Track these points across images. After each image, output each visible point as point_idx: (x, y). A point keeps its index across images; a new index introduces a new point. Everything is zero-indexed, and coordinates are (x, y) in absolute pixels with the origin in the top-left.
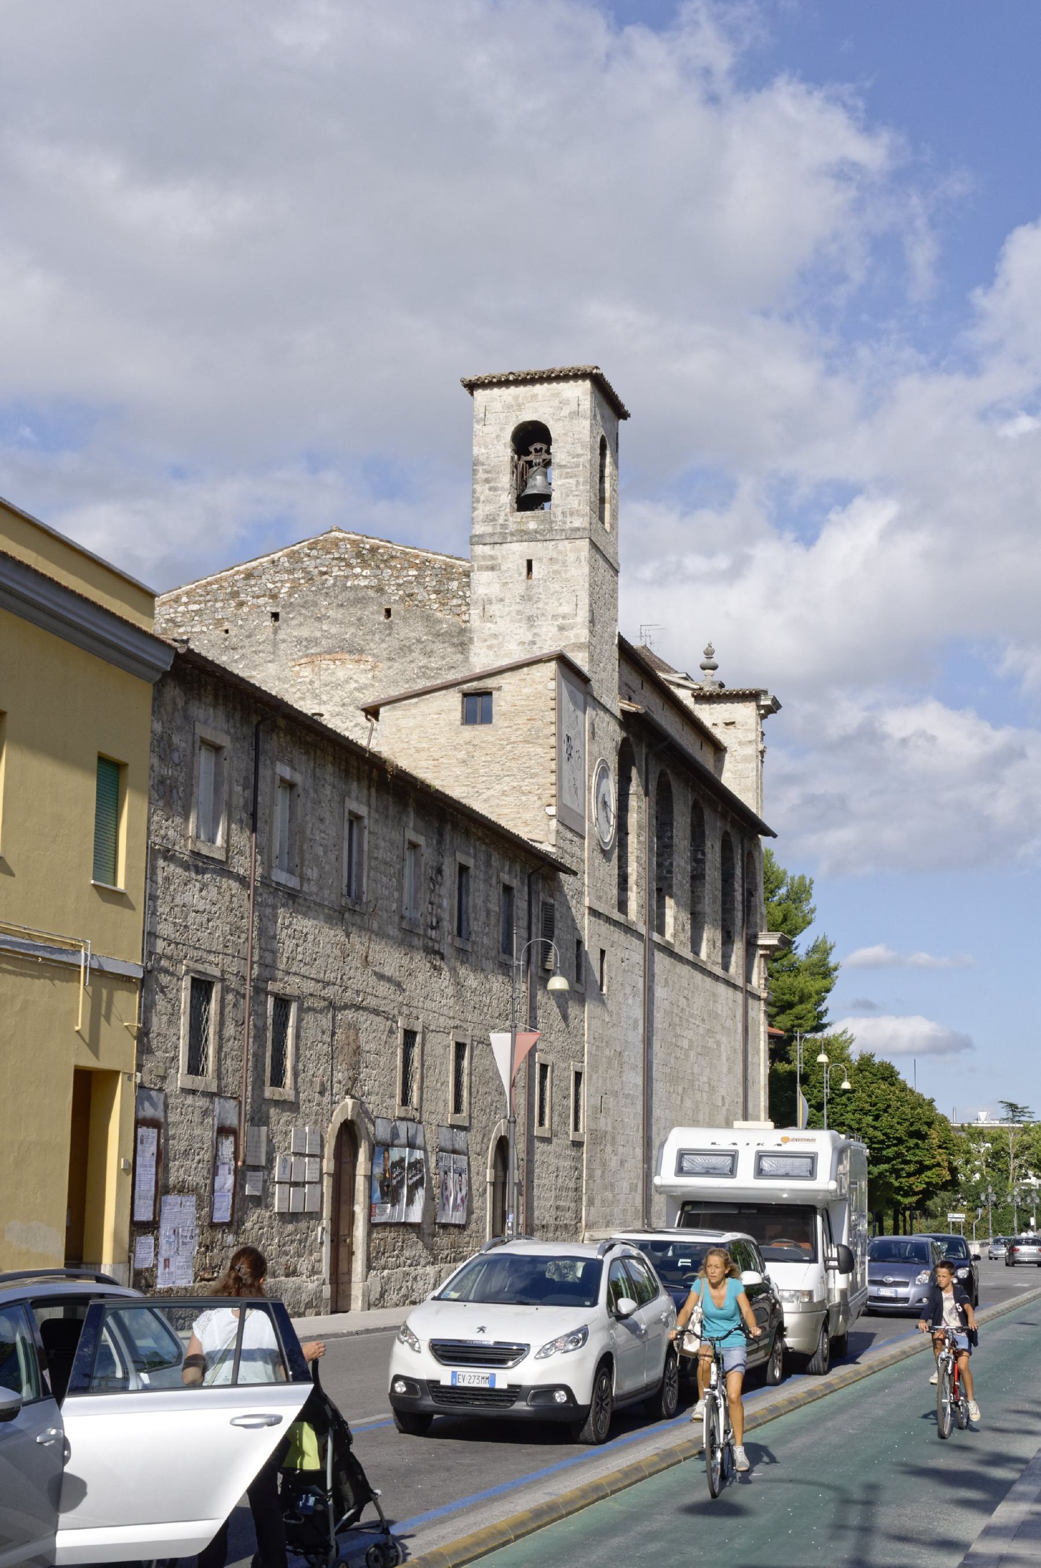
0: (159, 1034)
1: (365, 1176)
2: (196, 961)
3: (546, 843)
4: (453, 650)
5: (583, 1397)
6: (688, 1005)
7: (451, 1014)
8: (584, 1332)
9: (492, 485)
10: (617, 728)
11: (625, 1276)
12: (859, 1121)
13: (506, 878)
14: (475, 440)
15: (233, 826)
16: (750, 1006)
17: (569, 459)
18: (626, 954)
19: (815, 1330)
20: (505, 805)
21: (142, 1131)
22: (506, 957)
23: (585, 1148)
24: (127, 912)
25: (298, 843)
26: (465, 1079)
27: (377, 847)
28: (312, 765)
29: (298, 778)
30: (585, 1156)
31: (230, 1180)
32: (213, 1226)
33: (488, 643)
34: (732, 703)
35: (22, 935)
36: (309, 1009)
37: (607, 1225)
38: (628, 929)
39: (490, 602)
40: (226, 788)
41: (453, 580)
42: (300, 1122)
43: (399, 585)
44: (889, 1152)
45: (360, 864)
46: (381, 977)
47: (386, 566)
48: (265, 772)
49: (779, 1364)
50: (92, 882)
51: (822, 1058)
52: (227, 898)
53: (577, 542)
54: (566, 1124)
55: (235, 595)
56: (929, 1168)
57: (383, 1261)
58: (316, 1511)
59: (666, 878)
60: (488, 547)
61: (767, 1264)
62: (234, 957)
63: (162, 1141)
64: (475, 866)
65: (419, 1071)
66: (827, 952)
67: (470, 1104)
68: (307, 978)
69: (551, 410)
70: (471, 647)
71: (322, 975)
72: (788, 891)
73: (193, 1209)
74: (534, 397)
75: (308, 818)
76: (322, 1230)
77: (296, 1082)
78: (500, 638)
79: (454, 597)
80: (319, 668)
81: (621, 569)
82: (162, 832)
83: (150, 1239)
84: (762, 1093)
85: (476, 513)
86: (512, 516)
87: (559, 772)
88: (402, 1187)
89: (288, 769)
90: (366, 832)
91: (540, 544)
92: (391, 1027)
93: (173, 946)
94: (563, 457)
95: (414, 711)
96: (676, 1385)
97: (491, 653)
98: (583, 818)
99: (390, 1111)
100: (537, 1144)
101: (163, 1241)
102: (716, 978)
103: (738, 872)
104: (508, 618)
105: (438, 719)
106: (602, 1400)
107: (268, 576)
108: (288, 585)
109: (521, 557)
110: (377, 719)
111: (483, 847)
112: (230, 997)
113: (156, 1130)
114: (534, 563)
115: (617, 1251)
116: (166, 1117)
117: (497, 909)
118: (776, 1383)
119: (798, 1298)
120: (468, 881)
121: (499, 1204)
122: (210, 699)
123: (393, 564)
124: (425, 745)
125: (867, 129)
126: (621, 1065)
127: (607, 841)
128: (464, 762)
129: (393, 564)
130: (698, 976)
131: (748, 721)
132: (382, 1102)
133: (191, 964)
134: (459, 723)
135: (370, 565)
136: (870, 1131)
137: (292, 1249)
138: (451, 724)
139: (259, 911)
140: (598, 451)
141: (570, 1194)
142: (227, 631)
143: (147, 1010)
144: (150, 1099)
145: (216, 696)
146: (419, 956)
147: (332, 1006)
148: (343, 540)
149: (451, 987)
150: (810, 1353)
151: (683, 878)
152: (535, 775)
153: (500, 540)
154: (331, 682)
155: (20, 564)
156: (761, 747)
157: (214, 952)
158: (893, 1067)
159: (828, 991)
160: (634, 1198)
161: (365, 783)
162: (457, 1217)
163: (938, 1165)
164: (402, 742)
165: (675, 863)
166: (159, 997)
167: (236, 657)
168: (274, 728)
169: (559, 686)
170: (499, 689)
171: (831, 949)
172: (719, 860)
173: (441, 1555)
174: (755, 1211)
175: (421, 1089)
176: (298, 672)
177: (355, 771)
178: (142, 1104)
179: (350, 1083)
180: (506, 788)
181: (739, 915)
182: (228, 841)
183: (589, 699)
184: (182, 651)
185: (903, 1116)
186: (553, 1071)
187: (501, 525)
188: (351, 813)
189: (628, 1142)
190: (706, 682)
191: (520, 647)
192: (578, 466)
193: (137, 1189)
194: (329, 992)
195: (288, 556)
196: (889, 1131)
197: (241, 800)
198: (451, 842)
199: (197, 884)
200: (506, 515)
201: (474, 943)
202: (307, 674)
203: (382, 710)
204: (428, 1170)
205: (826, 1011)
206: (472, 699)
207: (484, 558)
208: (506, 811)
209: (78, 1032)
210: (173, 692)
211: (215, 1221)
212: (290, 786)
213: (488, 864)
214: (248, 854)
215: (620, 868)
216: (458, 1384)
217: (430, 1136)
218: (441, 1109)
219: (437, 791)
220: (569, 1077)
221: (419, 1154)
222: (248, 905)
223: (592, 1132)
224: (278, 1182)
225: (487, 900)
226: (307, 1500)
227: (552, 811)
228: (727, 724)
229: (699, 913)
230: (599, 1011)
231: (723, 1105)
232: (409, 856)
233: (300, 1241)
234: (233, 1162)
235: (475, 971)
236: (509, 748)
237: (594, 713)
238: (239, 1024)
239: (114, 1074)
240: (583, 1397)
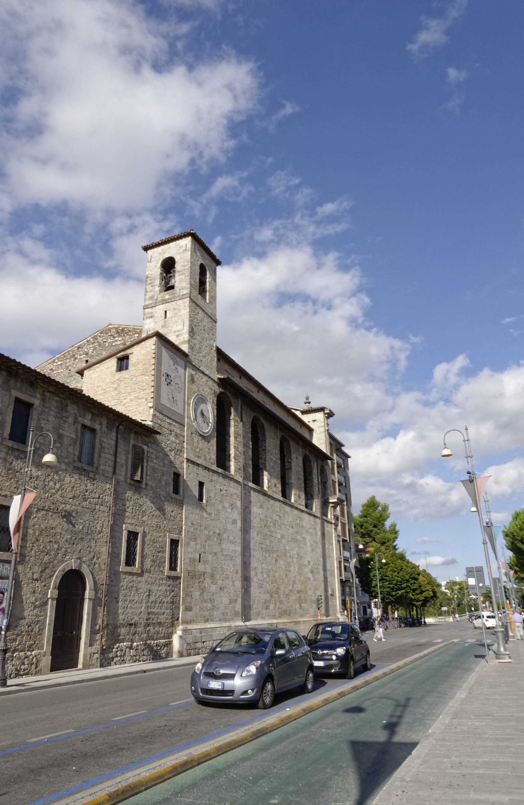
3: (148, 421)
9: (153, 284)
20: (131, 406)
23: (182, 580)
47: (127, 335)
55: (74, 355)
56: (424, 591)
60: (150, 309)
69: (176, 251)
74: (169, 248)
86: (160, 295)
91: (170, 304)
95: (97, 370)
98: (183, 416)
105: (107, 371)
107: (85, 347)
108: (92, 349)
109: (162, 310)
123: (129, 333)
124: (101, 384)
128: (116, 388)
129: (129, 333)
135: (121, 336)
136: (396, 578)
152: (145, 389)
156: (327, 428)
159: (397, 538)
163: (428, 590)
164: (92, 384)
165: (267, 457)
167: (72, 379)
170: (132, 353)
180: (132, 398)
187: (156, 299)
190: (306, 407)
192: (185, 270)
195: (93, 338)
207: (148, 314)
208: (132, 408)
228: (314, 421)
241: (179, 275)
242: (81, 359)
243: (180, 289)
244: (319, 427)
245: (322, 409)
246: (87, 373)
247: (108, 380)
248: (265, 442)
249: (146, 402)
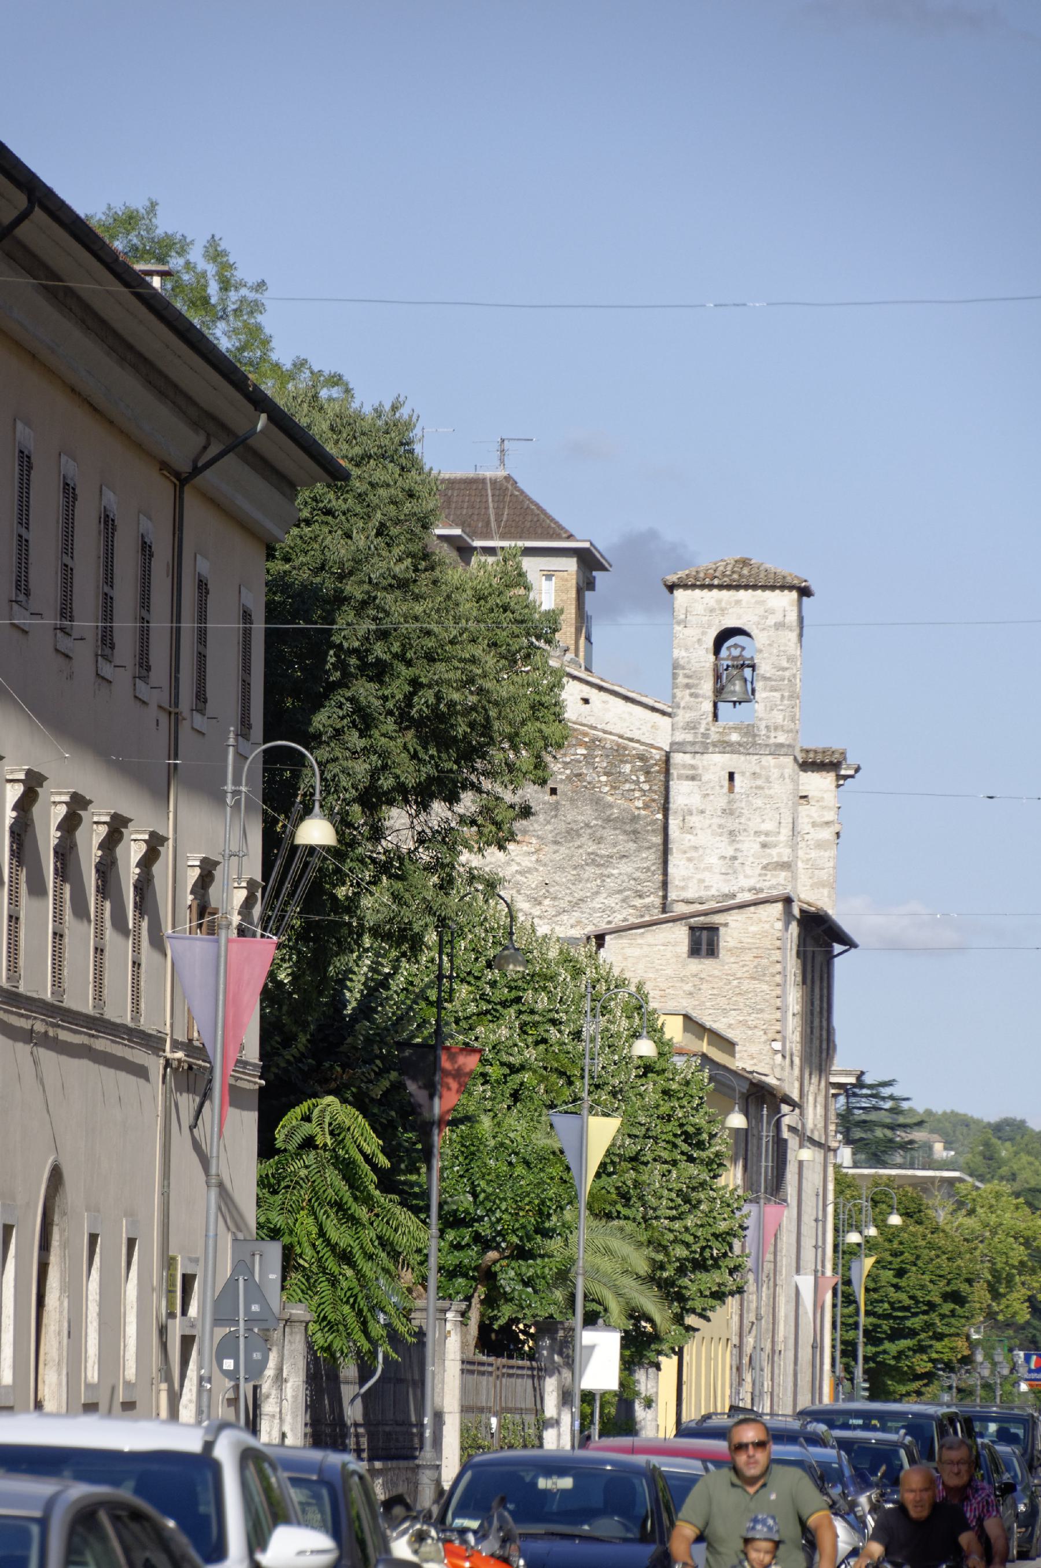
3: (772, 1076)
4: (625, 837)
9: (693, 691)
14: (676, 642)
33: (688, 855)
39: (691, 813)
41: (626, 762)
43: (566, 763)
44: (915, 1323)
53: (782, 758)
60: (688, 756)
69: (756, 619)
78: (701, 851)
94: (768, 669)
95: (640, 941)
97: (691, 865)
104: (709, 831)
105: (665, 950)
109: (723, 769)
114: (736, 776)
124: (651, 975)
128: (691, 994)
131: (825, 796)
134: (685, 955)
170: (726, 925)
180: (732, 1022)
185: (939, 1272)
191: (721, 862)
200: (708, 724)
203: (607, 938)
207: (684, 766)
236: (735, 983)
241: (765, 689)
244: (814, 824)
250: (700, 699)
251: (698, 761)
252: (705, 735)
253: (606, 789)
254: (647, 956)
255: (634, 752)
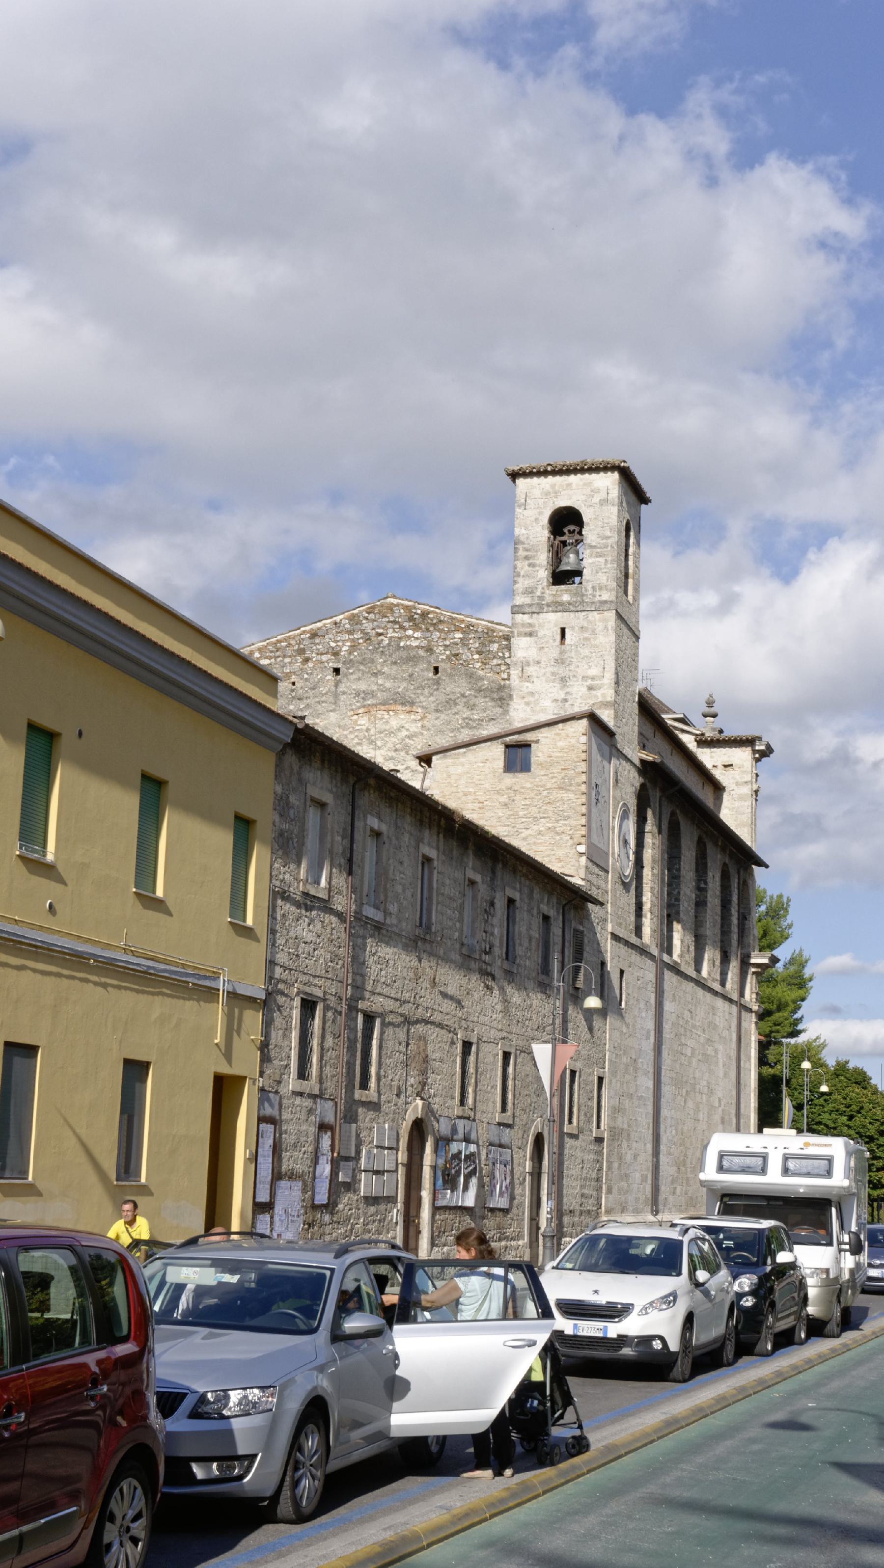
0: (276, 1046)
1: (431, 1166)
2: (305, 984)
3: (577, 877)
4: (493, 704)
5: (674, 1345)
6: (692, 1018)
7: (500, 1027)
8: (674, 1295)
9: (531, 561)
10: (636, 774)
11: (698, 1254)
12: (835, 1121)
13: (545, 909)
14: (517, 522)
15: (334, 870)
16: (743, 1018)
17: (599, 540)
18: (640, 973)
19: (831, 1302)
20: (541, 843)
21: (263, 1126)
22: (544, 977)
24: (254, 944)
25: (383, 883)
26: (510, 1083)
27: (443, 885)
28: (394, 816)
29: (384, 828)
30: (605, 1150)
31: (327, 1169)
32: (315, 1207)
33: (526, 700)
34: (731, 747)
35: (176, 965)
36: (390, 1024)
37: (623, 1211)
38: (642, 951)
39: (528, 664)
40: (329, 838)
41: (494, 642)
42: (381, 1120)
45: (430, 899)
46: (445, 995)
48: (359, 824)
49: (804, 1328)
50: (229, 920)
51: (806, 1065)
52: (329, 930)
54: (589, 1121)
55: (301, 652)
57: (443, 1240)
58: (538, 1410)
59: (674, 905)
61: (795, 1246)
62: (333, 980)
63: (277, 1135)
64: (521, 899)
65: (474, 1076)
66: (803, 965)
67: (514, 1104)
68: (389, 997)
69: (584, 498)
70: (511, 703)
71: (399, 994)
72: (767, 909)
73: (299, 1193)
75: (391, 861)
76: (396, 1213)
77: (379, 1086)
78: (537, 696)
79: (495, 657)
80: (375, 717)
81: (642, 636)
82: (281, 877)
83: (267, 1217)
84: (752, 1095)
85: (517, 586)
87: (588, 815)
88: (459, 1175)
89: (376, 820)
90: (435, 872)
91: (572, 614)
92: (452, 1039)
93: (287, 972)
94: (593, 538)
95: (462, 760)
96: (733, 1340)
97: (528, 709)
98: (607, 854)
99: (450, 1110)
100: (567, 1139)
101: (276, 1218)
102: (715, 993)
103: (735, 899)
104: (544, 679)
105: (483, 767)
106: (686, 1348)
107: (331, 636)
108: (348, 644)
109: (556, 625)
110: (430, 766)
111: (528, 882)
112: (330, 1014)
113: (273, 1126)
114: (567, 630)
115: (692, 1233)
116: (280, 1115)
117: (537, 936)
118: (802, 1343)
119: (817, 1275)
120: (514, 913)
121: (535, 1192)
122: (317, 764)
123: (441, 627)
124: (471, 790)
125: (849, 202)
126: (636, 1070)
127: (626, 874)
128: (506, 805)
129: (441, 627)
130: (700, 992)
132: (445, 1103)
133: (301, 987)
135: (421, 628)
137: (373, 1227)
138: (494, 772)
139: (353, 941)
140: (624, 533)
141: (593, 1183)
142: (294, 684)
143: (268, 1024)
144: (269, 1100)
145: (323, 761)
146: (475, 977)
147: (408, 1021)
148: (397, 605)
149: (500, 1004)
150: (826, 1319)
151: (689, 905)
153: (538, 609)
154: (385, 730)
155: (183, 660)
156: (755, 787)
157: (318, 977)
158: (865, 1073)
159: (803, 1000)
160: (644, 1188)
161: (435, 830)
162: (501, 1202)
164: (452, 786)
165: (682, 892)
166: (276, 1015)
168: (367, 786)
169: (589, 740)
170: (537, 742)
171: (806, 962)
172: (719, 888)
173: (616, 1445)
174: (781, 1203)
175: (475, 1092)
176: (356, 721)
177: (427, 820)
178: (263, 1105)
179: (420, 1087)
180: (542, 829)
181: (735, 937)
182: (330, 883)
183: (614, 751)
184: (300, 726)
186: (580, 1076)
188: (424, 856)
189: (640, 1138)
190: (709, 730)
191: (554, 704)
193: (258, 1176)
194: (405, 1009)
196: (862, 1130)
197: (341, 848)
198: (502, 879)
199: (306, 919)
201: (519, 965)
202: (363, 722)
203: (434, 758)
204: (480, 1161)
205: (802, 1017)
206: (513, 750)
207: (523, 625)
209: (217, 1044)
210: (291, 759)
211: (316, 1203)
212: (377, 834)
213: (531, 896)
214: (345, 893)
215: (637, 897)
216: (579, 1334)
217: (483, 1133)
218: (490, 1109)
219: (494, 836)
220: (593, 1081)
221: (473, 1148)
222: (344, 936)
223: (611, 1129)
224: (364, 1171)
225: (529, 928)
226: (532, 1402)
227: (582, 849)
228: (725, 766)
229: (702, 936)
230: (618, 1023)
231: (720, 1106)
232: (469, 893)
233: (380, 1221)
234: (330, 1153)
235: (519, 990)
237: (618, 763)
238: (337, 1036)
239: (242, 1080)
240: (674, 1345)
241: (591, 556)
242: (322, 662)
243: (594, 588)
245: (748, 742)
246: (440, 761)
247: (487, 786)
248: (680, 861)
249: (571, 842)
250: (537, 568)
251: (534, 620)
252: (541, 598)
253: (478, 665)
254: (468, 773)
255: (501, 634)
